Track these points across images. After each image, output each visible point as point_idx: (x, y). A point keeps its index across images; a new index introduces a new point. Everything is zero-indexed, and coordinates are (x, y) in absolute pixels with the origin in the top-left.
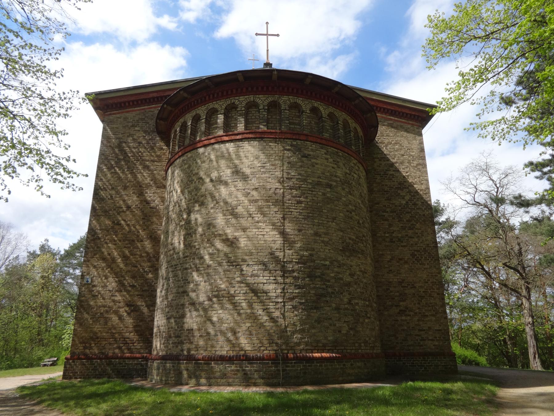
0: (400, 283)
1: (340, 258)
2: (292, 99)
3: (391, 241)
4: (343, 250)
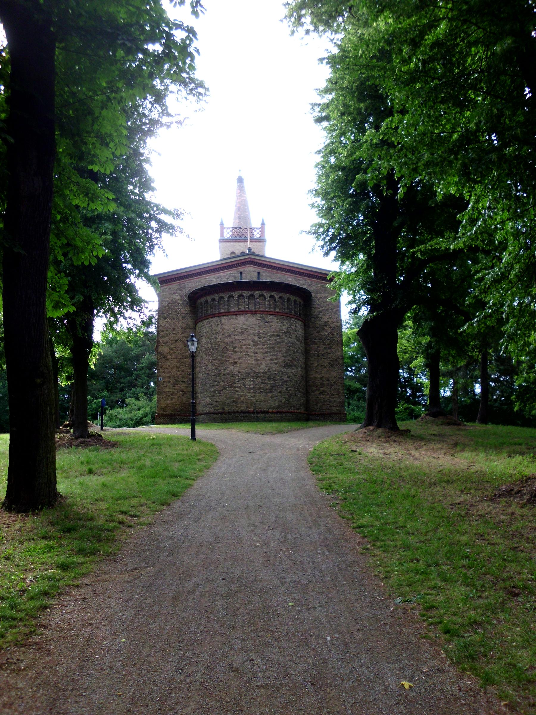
0: (321, 378)
1: (283, 370)
2: (261, 292)
3: (318, 356)
4: (284, 366)
